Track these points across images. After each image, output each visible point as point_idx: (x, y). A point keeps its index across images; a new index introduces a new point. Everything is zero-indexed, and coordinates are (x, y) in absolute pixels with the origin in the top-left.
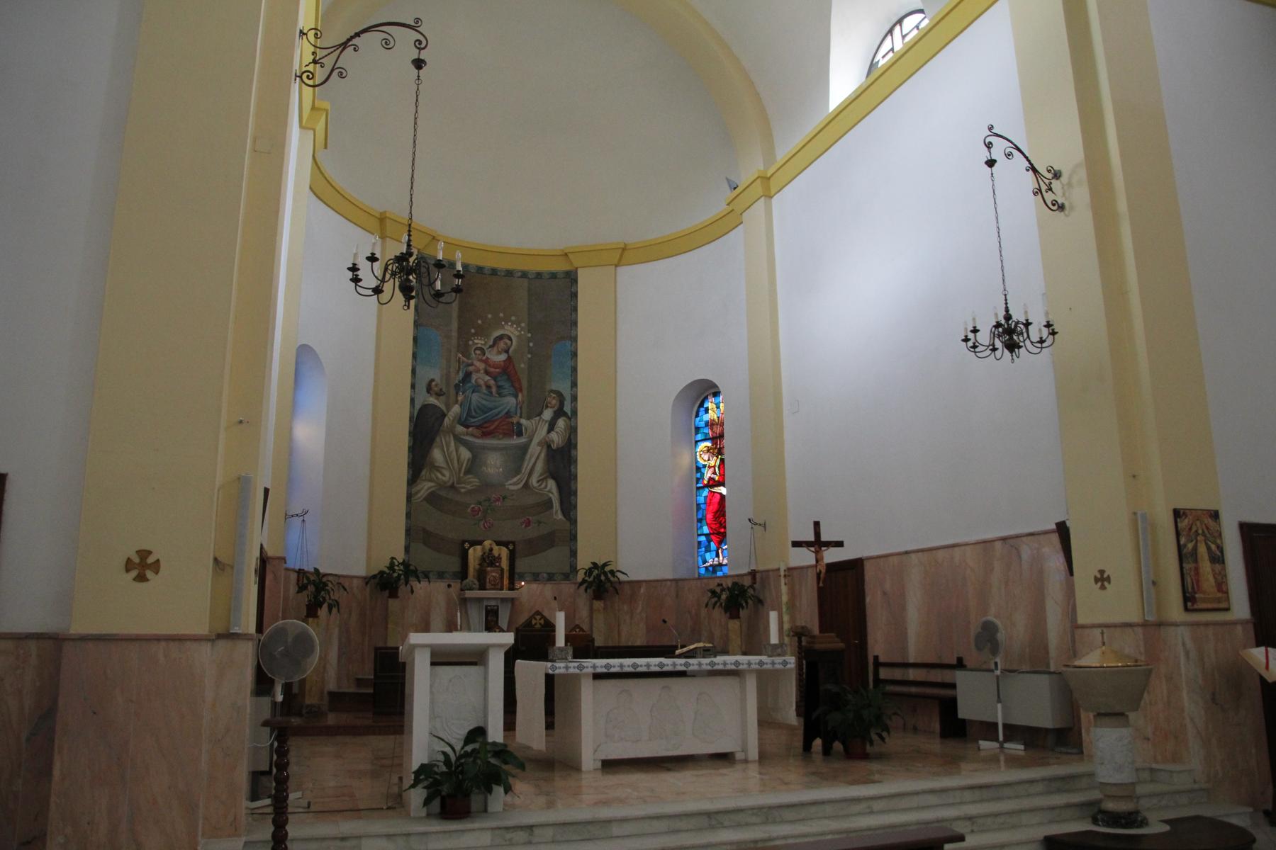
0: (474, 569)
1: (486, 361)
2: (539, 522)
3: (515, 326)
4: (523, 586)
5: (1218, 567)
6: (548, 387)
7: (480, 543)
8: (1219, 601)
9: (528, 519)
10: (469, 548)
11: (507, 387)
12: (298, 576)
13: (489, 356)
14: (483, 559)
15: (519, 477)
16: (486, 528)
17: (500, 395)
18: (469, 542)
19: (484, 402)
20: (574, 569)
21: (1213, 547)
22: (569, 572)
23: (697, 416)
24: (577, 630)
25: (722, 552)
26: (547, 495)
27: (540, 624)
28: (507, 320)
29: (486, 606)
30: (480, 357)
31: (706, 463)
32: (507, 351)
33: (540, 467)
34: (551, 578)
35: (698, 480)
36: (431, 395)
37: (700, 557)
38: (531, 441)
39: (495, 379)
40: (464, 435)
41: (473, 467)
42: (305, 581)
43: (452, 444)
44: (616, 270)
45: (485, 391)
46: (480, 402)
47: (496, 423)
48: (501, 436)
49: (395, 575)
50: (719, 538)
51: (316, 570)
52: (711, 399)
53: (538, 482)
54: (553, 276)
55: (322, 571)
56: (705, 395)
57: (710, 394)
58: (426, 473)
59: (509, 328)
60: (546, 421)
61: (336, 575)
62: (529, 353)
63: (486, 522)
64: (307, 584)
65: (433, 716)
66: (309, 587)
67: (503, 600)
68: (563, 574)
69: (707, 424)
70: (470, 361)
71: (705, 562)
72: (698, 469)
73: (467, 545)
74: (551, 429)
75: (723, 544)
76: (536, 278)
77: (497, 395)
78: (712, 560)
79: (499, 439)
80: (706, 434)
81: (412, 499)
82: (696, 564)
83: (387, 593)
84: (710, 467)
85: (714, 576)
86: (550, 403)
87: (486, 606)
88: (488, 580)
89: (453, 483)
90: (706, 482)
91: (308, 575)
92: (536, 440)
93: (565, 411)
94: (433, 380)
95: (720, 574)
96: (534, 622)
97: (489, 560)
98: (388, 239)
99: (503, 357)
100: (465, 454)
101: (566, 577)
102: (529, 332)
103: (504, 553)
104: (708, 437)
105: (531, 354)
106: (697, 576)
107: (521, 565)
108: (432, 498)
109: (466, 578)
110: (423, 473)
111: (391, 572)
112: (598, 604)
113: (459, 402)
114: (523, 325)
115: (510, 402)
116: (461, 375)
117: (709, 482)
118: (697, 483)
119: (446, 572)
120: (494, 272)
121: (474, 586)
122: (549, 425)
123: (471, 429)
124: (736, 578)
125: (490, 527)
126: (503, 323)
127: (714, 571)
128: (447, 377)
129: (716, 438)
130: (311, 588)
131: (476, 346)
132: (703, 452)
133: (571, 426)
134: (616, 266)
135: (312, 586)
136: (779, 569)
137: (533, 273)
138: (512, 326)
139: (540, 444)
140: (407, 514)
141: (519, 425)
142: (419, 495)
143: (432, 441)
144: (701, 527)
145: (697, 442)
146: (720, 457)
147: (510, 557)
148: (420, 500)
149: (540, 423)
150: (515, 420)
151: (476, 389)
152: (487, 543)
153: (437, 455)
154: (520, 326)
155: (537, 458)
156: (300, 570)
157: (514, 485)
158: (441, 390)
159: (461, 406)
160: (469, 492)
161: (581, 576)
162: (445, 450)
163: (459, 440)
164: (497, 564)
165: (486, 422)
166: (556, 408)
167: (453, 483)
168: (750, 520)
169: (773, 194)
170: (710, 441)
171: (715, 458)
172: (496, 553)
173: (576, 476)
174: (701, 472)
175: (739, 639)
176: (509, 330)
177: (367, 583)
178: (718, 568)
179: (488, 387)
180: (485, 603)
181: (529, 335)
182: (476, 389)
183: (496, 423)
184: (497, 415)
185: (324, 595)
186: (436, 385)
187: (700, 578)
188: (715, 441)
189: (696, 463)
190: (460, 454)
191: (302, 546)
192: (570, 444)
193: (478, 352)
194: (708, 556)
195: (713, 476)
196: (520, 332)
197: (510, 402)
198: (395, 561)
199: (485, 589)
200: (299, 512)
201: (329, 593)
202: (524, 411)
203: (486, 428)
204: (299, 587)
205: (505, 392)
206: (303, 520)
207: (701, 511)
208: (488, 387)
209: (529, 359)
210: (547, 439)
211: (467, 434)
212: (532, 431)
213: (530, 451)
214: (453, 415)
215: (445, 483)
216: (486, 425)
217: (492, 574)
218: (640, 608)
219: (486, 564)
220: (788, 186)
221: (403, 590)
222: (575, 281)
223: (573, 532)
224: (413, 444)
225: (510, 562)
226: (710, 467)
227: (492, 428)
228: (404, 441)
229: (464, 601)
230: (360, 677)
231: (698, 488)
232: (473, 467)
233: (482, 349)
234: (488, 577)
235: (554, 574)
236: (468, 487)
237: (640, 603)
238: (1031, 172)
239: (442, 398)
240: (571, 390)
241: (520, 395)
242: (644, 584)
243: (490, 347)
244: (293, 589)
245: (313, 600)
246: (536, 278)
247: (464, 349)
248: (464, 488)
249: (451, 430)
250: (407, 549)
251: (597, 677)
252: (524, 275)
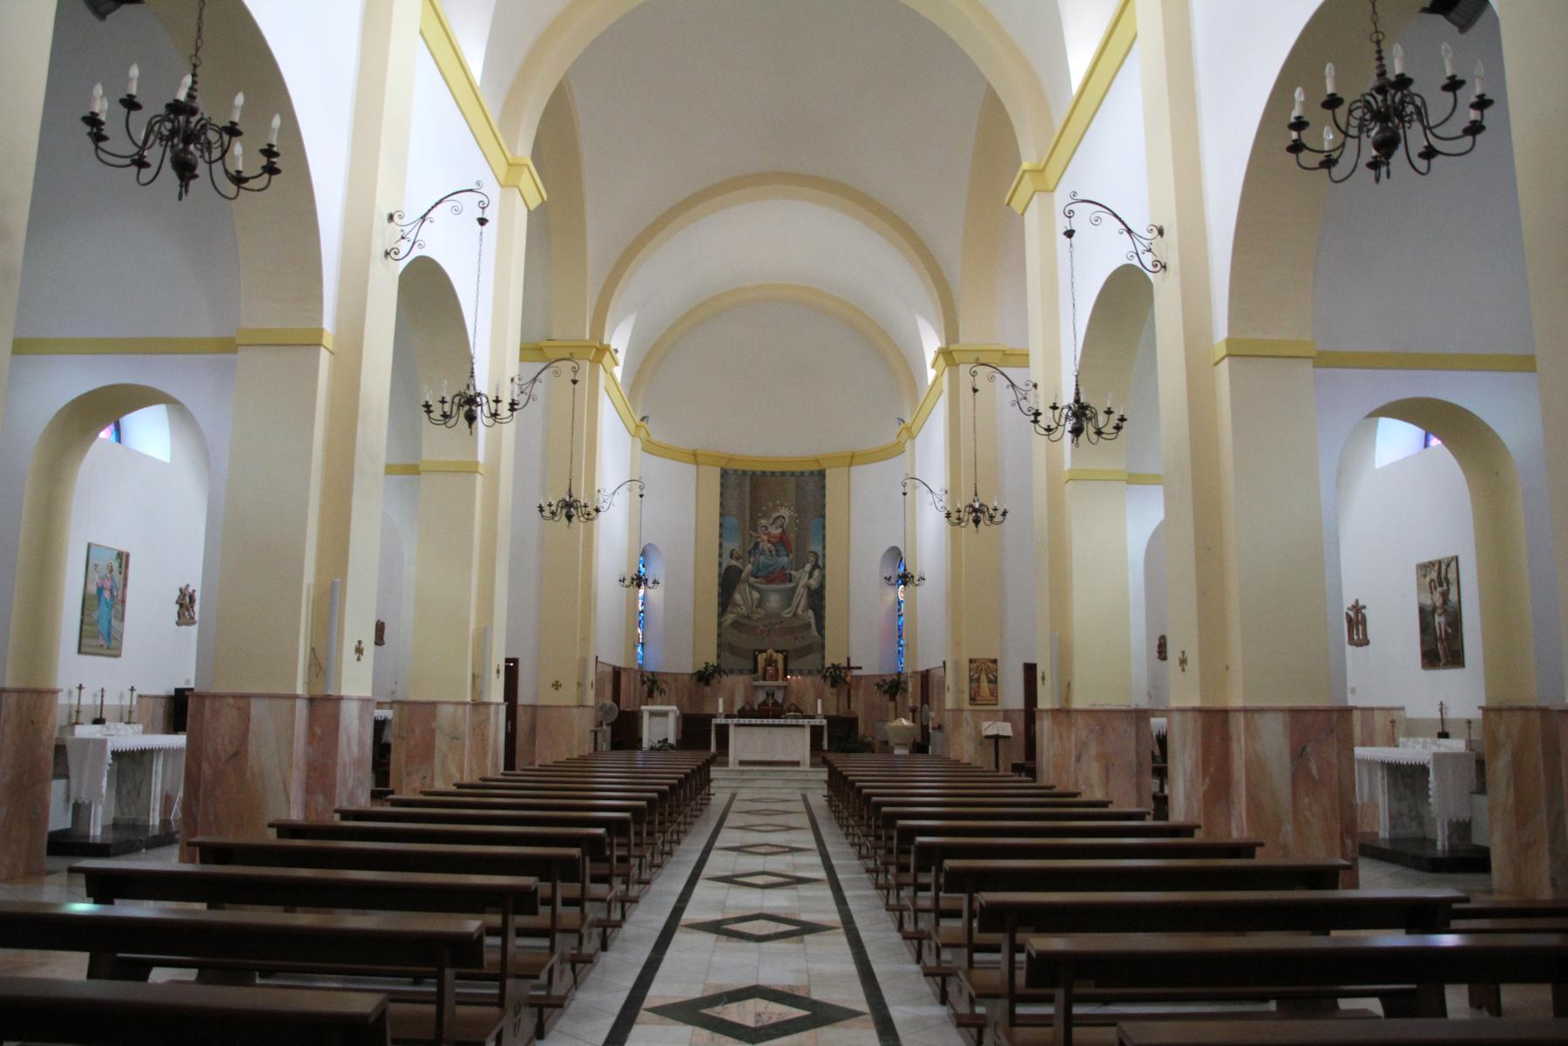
1: (768, 534)
2: (803, 637)
5: (992, 685)
7: (765, 651)
8: (990, 700)
15: (790, 609)
17: (778, 556)
20: (823, 667)
21: (991, 676)
28: (782, 506)
32: (782, 526)
33: (803, 602)
34: (810, 673)
38: (797, 585)
39: (774, 545)
41: (761, 603)
43: (748, 589)
54: (812, 473)
65: (650, 733)
67: (779, 687)
72: (899, 603)
93: (819, 566)
97: (770, 662)
99: (779, 531)
100: (756, 595)
103: (780, 657)
107: (791, 666)
108: (735, 624)
115: (784, 560)
116: (752, 545)
120: (773, 474)
123: (759, 580)
139: (803, 587)
141: (791, 575)
150: (787, 572)
151: (762, 553)
152: (769, 651)
153: (737, 597)
157: (787, 614)
163: (752, 587)
176: (784, 512)
179: (770, 551)
181: (796, 515)
182: (762, 553)
192: (822, 586)
197: (784, 560)
205: (781, 554)
208: (770, 551)
213: (798, 590)
217: (770, 670)
221: (714, 682)
232: (761, 603)
236: (759, 616)
238: (1126, 234)
239: (741, 561)
243: (772, 524)
247: (754, 528)
249: (746, 581)
251: (738, 725)
252: (793, 474)
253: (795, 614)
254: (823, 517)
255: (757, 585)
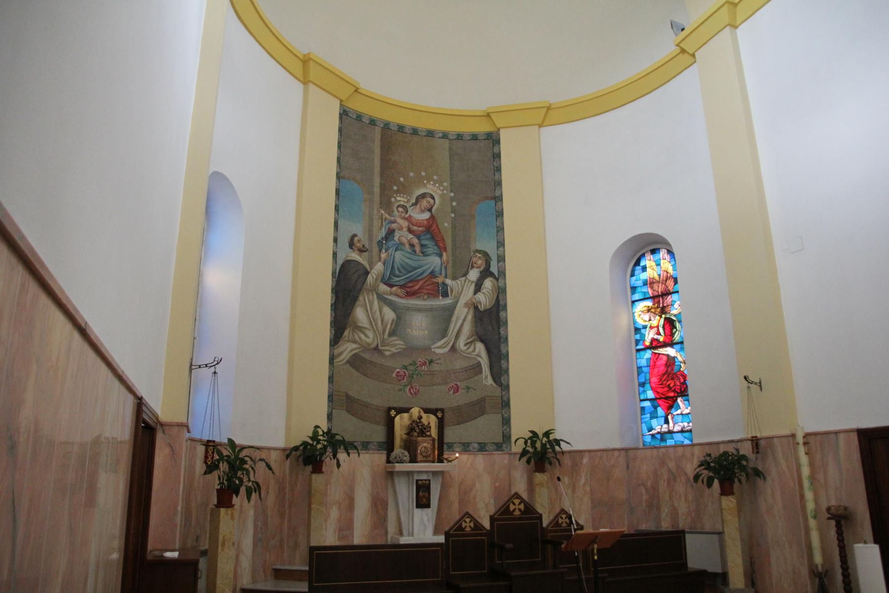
0: (401, 439)
1: (409, 219)
2: (468, 388)
3: (437, 185)
4: (457, 458)
6: (473, 248)
7: (407, 410)
9: (456, 385)
10: (396, 416)
11: (431, 248)
12: (207, 452)
13: (412, 215)
14: (410, 430)
16: (412, 394)
17: (424, 254)
18: (394, 409)
19: (407, 261)
20: (507, 437)
22: (501, 441)
23: (632, 275)
24: (564, 516)
25: (672, 418)
26: (475, 359)
27: (520, 510)
28: (429, 179)
29: (417, 481)
30: (403, 215)
31: (646, 323)
32: (430, 210)
33: (467, 329)
34: (482, 447)
35: (637, 342)
36: (354, 251)
37: (644, 425)
38: (457, 302)
39: (418, 238)
40: (387, 295)
42: (217, 457)
44: (539, 130)
45: (409, 250)
46: (403, 261)
47: (421, 283)
48: (426, 297)
49: (319, 446)
50: (668, 403)
51: (231, 441)
52: (649, 256)
53: (466, 345)
54: (475, 137)
55: (238, 441)
56: (642, 252)
57: (648, 251)
58: (349, 334)
59: (431, 186)
60: (472, 282)
61: (732, 441)
62: (452, 212)
63: (412, 388)
64: (218, 461)
66: (221, 465)
67: (435, 473)
68: (496, 444)
69: (645, 283)
70: (392, 218)
71: (650, 429)
73: (393, 413)
74: (478, 288)
75: (673, 410)
76: (457, 139)
77: (421, 254)
78: (660, 427)
79: (424, 300)
80: (645, 293)
81: (335, 361)
82: (640, 430)
83: (309, 468)
84: (651, 328)
85: (663, 444)
86: (475, 263)
87: (417, 481)
88: (419, 451)
89: (378, 345)
90: (647, 343)
91: (219, 447)
92: (463, 301)
94: (355, 236)
95: (670, 442)
96: (512, 507)
97: (417, 429)
98: (311, 85)
99: (426, 215)
100: (390, 315)
101: (499, 447)
102: (451, 191)
103: (431, 420)
104: (648, 296)
105: (454, 213)
106: (641, 446)
107: (451, 434)
108: (356, 362)
109: (392, 450)
110: (346, 333)
111: (315, 443)
112: (539, 477)
113: (382, 260)
114: (445, 184)
115: (434, 262)
116: (383, 233)
117: (651, 343)
118: (637, 345)
119: (370, 442)
120: (415, 131)
121: (405, 458)
122: (476, 285)
123: (394, 289)
124: (707, 447)
125: (415, 393)
126: (425, 182)
127: (663, 439)
128: (370, 233)
129: (658, 296)
130: (224, 467)
131: (398, 204)
132: (642, 312)
133: (499, 288)
134: (540, 126)
135: (225, 463)
136: (793, 436)
137: (453, 135)
138: (434, 185)
139: (466, 305)
140: (329, 378)
142: (342, 357)
143: (356, 299)
144: (644, 391)
145: (633, 302)
146: (663, 316)
147: (439, 426)
148: (342, 363)
149: (466, 283)
150: (440, 280)
151: (399, 247)
152: (415, 411)
153: (360, 314)
154: (442, 186)
155: (464, 320)
156: (209, 441)
158: (364, 246)
159: (384, 264)
160: (393, 355)
161: (518, 448)
162: (369, 310)
163: (382, 298)
164: (428, 433)
165: (411, 281)
166: (482, 269)
167: (378, 345)
168: (745, 378)
169: (738, 24)
170: (650, 300)
171: (658, 318)
172: (424, 420)
173: (507, 338)
174: (641, 333)
175: (737, 519)
177: (287, 456)
178: (668, 436)
180: (416, 477)
181: (452, 194)
182: (399, 247)
183: (421, 283)
184: (422, 274)
185: (242, 476)
186: (359, 241)
187: (646, 447)
188: (656, 300)
189: (634, 324)
190: (384, 315)
191: (212, 413)
193: (400, 209)
194: (654, 422)
195: (656, 337)
196: (442, 190)
197: (434, 262)
198: (319, 429)
199: (416, 462)
200: (209, 361)
201: (248, 474)
202: (449, 272)
203: (409, 287)
204: (207, 466)
206: (215, 373)
207: (642, 375)
209: (452, 218)
210: (474, 300)
211: (391, 294)
212: (458, 291)
214: (376, 273)
215: (369, 344)
216: (410, 285)
217: (424, 445)
218: (583, 480)
219: (415, 434)
220: (759, 12)
221: (328, 463)
222: (498, 142)
223: (505, 398)
224: (335, 302)
225: (439, 432)
226: (651, 328)
227: (417, 287)
228: (326, 298)
229: (391, 475)
230: (278, 567)
231: (638, 351)
233: (404, 207)
234: (419, 448)
235: (485, 444)
236: (394, 350)
237: (583, 474)
239: (366, 254)
240: (497, 250)
241: (444, 254)
242: (587, 454)
243: (413, 205)
244: (200, 467)
245: (226, 483)
246: (457, 139)
247: (386, 204)
248: (389, 350)
249: (374, 289)
250: (330, 417)
252: (445, 136)
253: (453, 349)
254: (499, 199)
255: (393, 298)
